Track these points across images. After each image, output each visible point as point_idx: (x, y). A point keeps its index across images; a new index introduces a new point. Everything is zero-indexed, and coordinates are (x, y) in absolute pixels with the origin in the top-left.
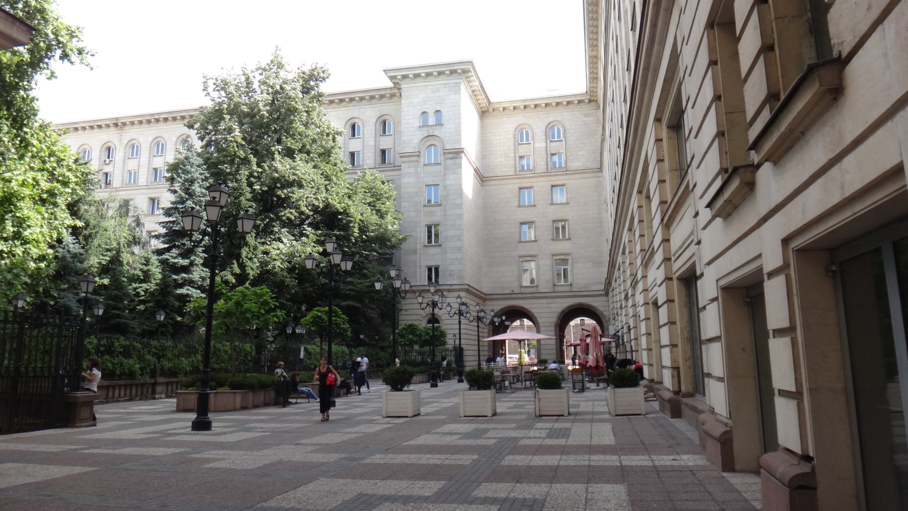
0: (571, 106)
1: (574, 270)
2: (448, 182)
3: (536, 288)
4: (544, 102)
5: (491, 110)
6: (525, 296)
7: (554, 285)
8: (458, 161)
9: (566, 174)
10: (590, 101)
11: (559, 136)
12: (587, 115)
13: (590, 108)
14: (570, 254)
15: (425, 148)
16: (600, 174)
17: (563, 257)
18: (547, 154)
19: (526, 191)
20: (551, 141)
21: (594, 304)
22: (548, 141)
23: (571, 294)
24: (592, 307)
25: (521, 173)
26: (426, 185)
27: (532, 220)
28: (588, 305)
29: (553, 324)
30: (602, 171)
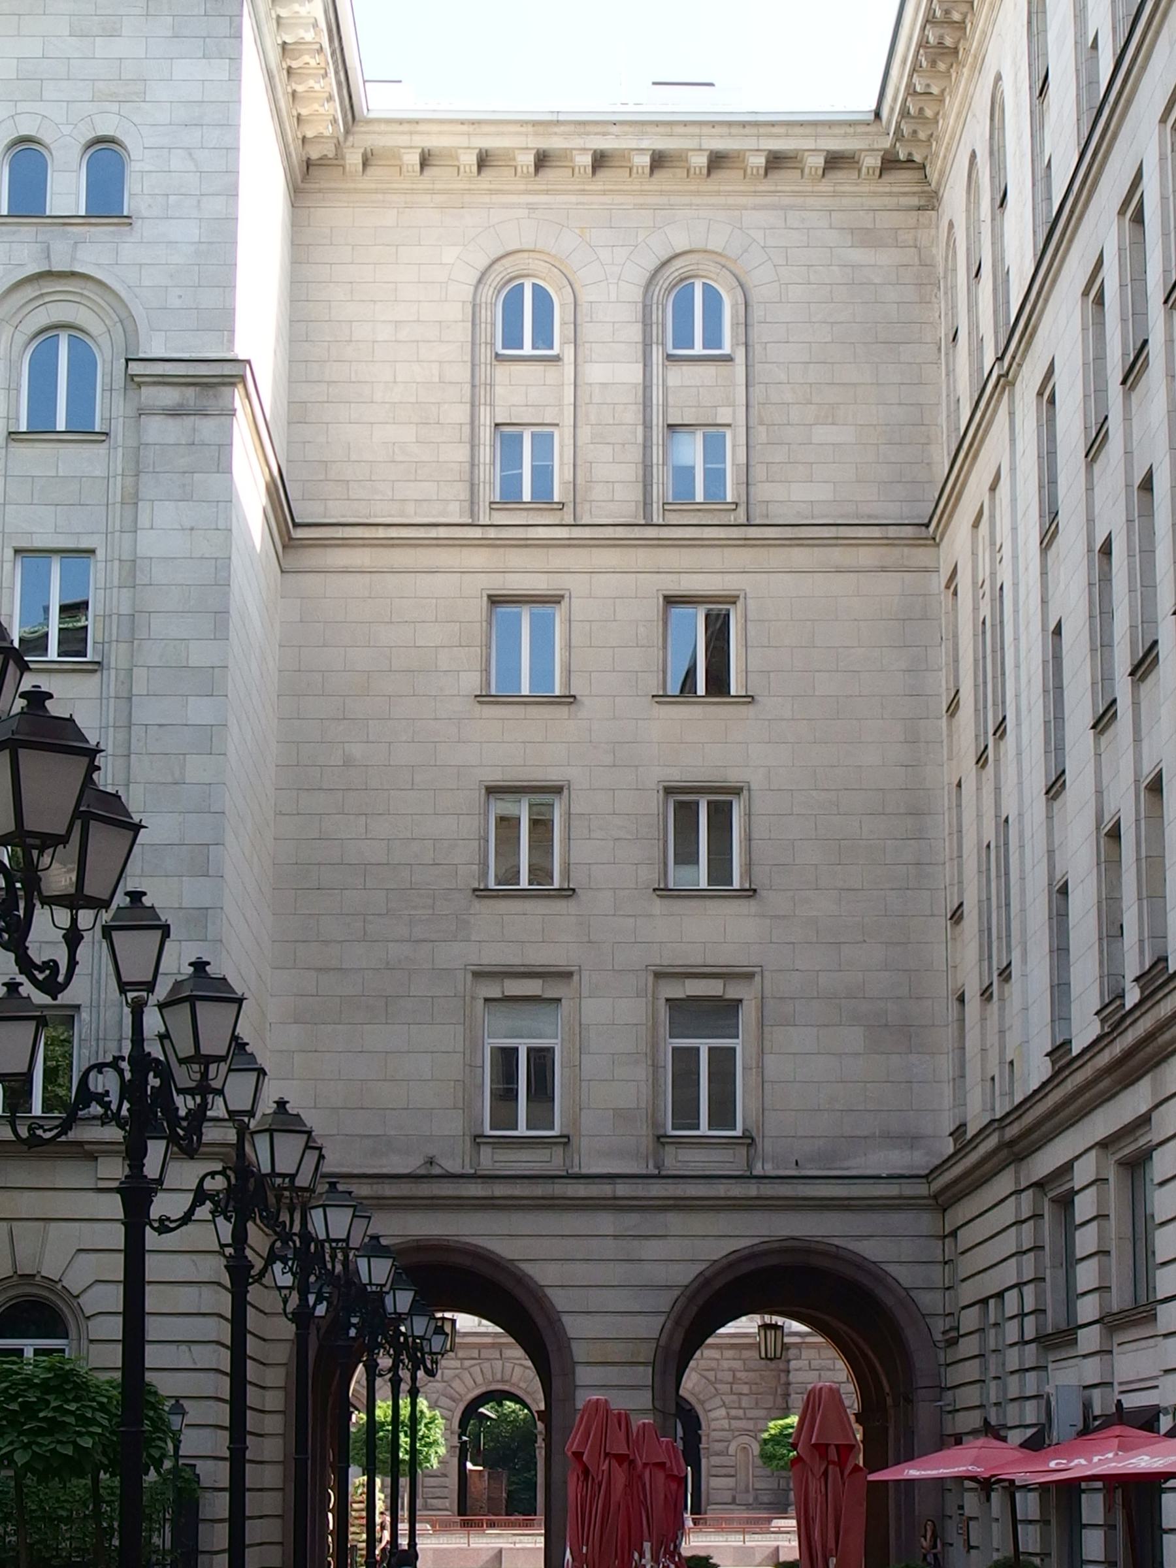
0: (785, 180)
1: (769, 1060)
2: (149, 544)
3: (559, 1150)
4: (645, 144)
5: (354, 159)
6: (500, 1190)
7: (661, 1140)
8: (207, 428)
9: (746, 543)
10: (890, 163)
11: (713, 337)
12: (867, 237)
13: (876, 202)
14: (750, 976)
15: (21, 339)
16: (921, 556)
17: (713, 988)
18: (647, 425)
19: (525, 615)
20: (670, 358)
21: (870, 1250)
22: (657, 355)
23: (752, 1190)
24: (860, 1263)
25: (500, 518)
26: (17, 551)
27: (553, 776)
28: (838, 1255)
29: (646, 1352)
30: (935, 541)
